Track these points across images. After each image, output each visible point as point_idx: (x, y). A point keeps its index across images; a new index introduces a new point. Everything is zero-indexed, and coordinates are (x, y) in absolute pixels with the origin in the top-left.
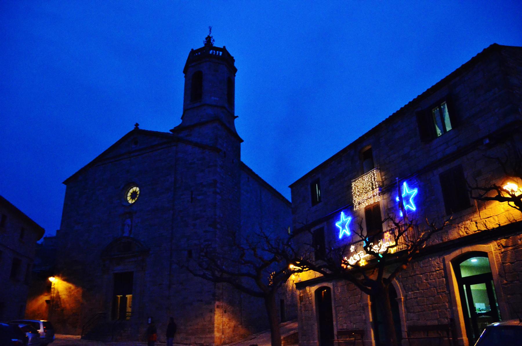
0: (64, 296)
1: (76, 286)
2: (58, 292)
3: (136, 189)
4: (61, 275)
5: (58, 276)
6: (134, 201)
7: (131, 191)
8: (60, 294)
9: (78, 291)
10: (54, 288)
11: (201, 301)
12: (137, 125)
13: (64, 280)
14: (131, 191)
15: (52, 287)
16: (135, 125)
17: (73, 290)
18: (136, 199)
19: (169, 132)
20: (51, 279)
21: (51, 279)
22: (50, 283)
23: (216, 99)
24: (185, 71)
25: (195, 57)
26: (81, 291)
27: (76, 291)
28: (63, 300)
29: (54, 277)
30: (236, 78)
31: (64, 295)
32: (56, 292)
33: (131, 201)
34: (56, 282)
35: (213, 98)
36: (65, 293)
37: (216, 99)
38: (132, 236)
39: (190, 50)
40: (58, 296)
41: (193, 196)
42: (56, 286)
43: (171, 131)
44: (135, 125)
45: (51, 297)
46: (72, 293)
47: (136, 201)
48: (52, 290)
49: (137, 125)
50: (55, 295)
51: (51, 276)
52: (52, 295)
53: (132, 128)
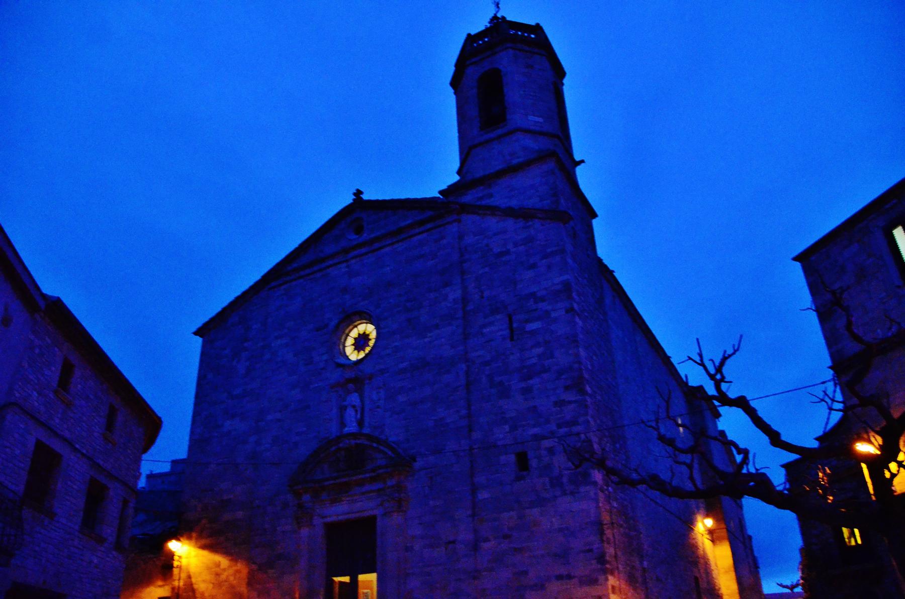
0: (202, 585)
1: (231, 560)
2: (189, 577)
3: (370, 329)
4: (194, 535)
5: (189, 538)
6: (362, 355)
7: (354, 333)
8: (193, 580)
9: (238, 571)
10: (180, 567)
11: (569, 577)
12: (358, 193)
13: (203, 547)
14: (354, 333)
15: (176, 563)
16: (354, 194)
17: (224, 570)
18: (368, 349)
19: (439, 195)
20: (173, 545)
21: (173, 545)
22: (171, 555)
23: (537, 119)
24: (455, 83)
25: (474, 49)
26: (245, 571)
27: (231, 571)
28: (202, 594)
29: (178, 540)
30: (566, 89)
31: (204, 581)
32: (183, 575)
33: (354, 356)
34: (184, 552)
35: (531, 118)
36: (208, 577)
37: (537, 119)
38: (366, 431)
39: (464, 36)
40: (190, 586)
41: (515, 325)
42: (184, 562)
43: (441, 192)
44: (354, 194)
45: (173, 589)
46: (224, 577)
47: (367, 355)
48: (176, 571)
49: (358, 193)
50: (182, 584)
51: (170, 539)
52: (176, 583)
53: (349, 199)
